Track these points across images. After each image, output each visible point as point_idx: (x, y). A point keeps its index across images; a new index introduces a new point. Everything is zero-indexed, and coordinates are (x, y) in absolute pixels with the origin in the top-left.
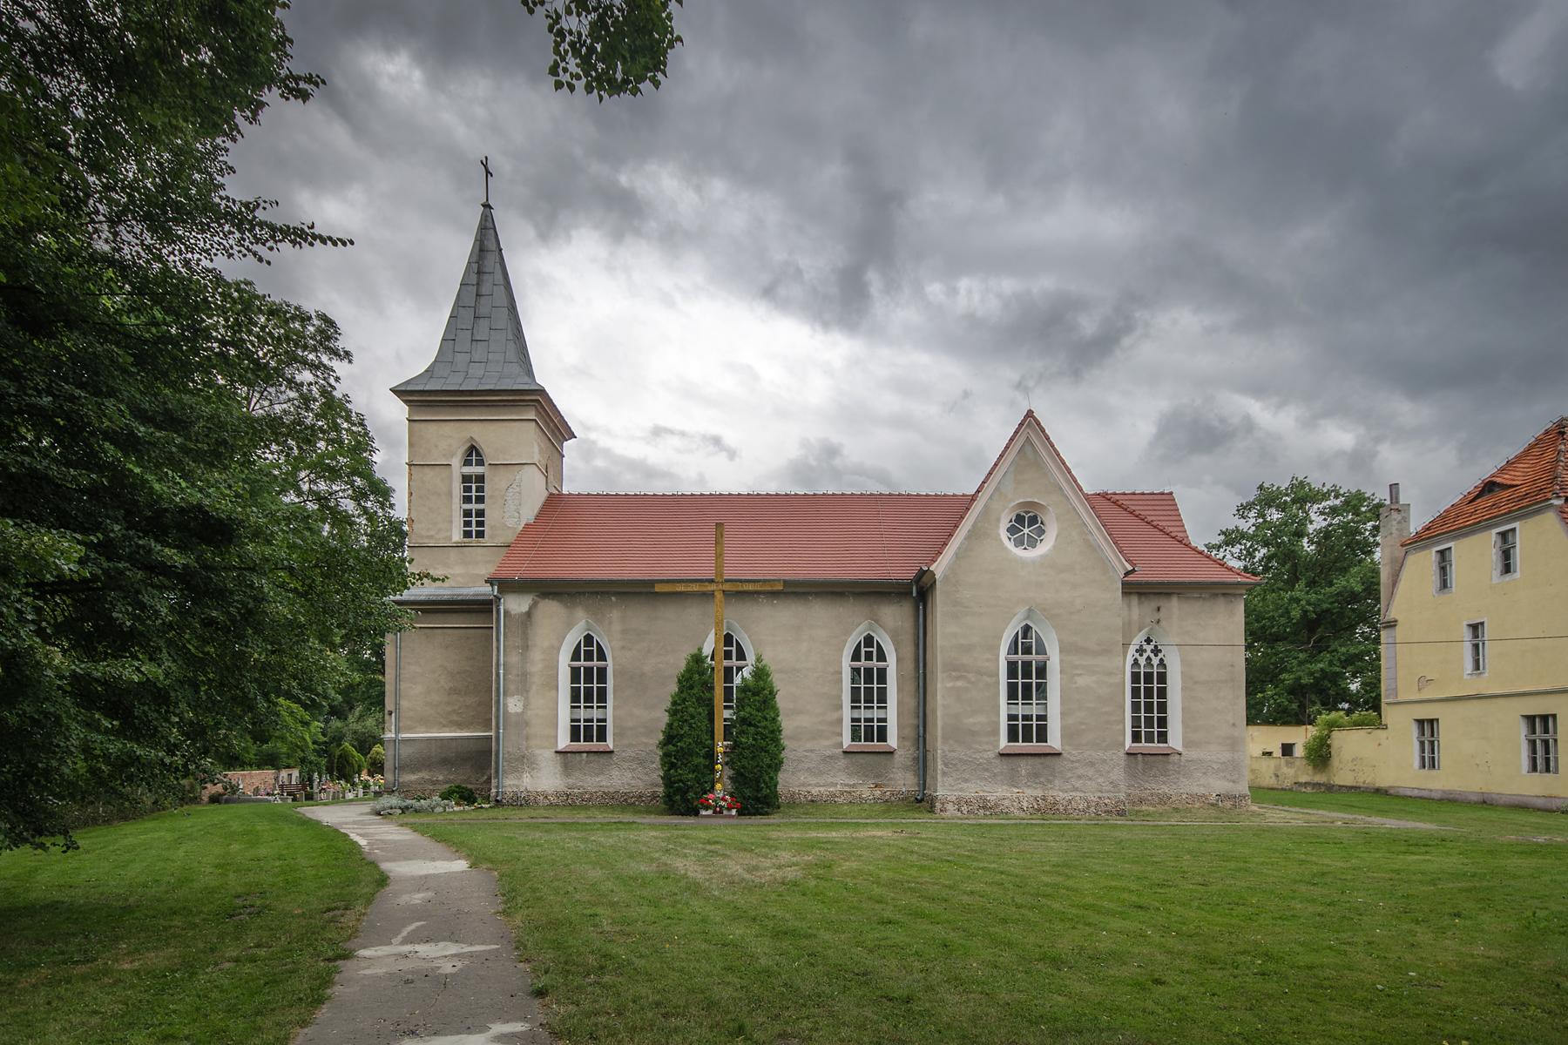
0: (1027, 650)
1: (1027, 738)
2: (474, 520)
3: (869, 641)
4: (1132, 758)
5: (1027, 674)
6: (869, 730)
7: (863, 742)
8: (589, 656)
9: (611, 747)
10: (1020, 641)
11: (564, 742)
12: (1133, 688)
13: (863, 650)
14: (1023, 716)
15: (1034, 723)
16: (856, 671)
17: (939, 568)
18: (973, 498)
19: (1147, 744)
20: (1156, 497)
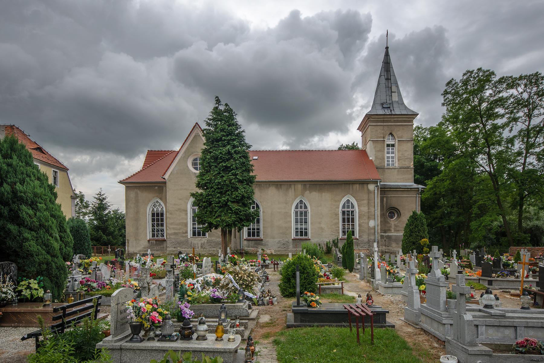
0: (348, 207)
1: (254, 235)
2: (390, 160)
3: (301, 202)
4: (295, 241)
5: (348, 215)
6: (301, 232)
7: (256, 237)
8: (348, 207)
9: (262, 238)
10: (346, 204)
11: (293, 236)
12: (152, 219)
13: (299, 205)
14: (198, 228)
15: (251, 231)
16: (296, 213)
17: (166, 176)
18: (178, 152)
19: (305, 237)
20: (162, 152)
